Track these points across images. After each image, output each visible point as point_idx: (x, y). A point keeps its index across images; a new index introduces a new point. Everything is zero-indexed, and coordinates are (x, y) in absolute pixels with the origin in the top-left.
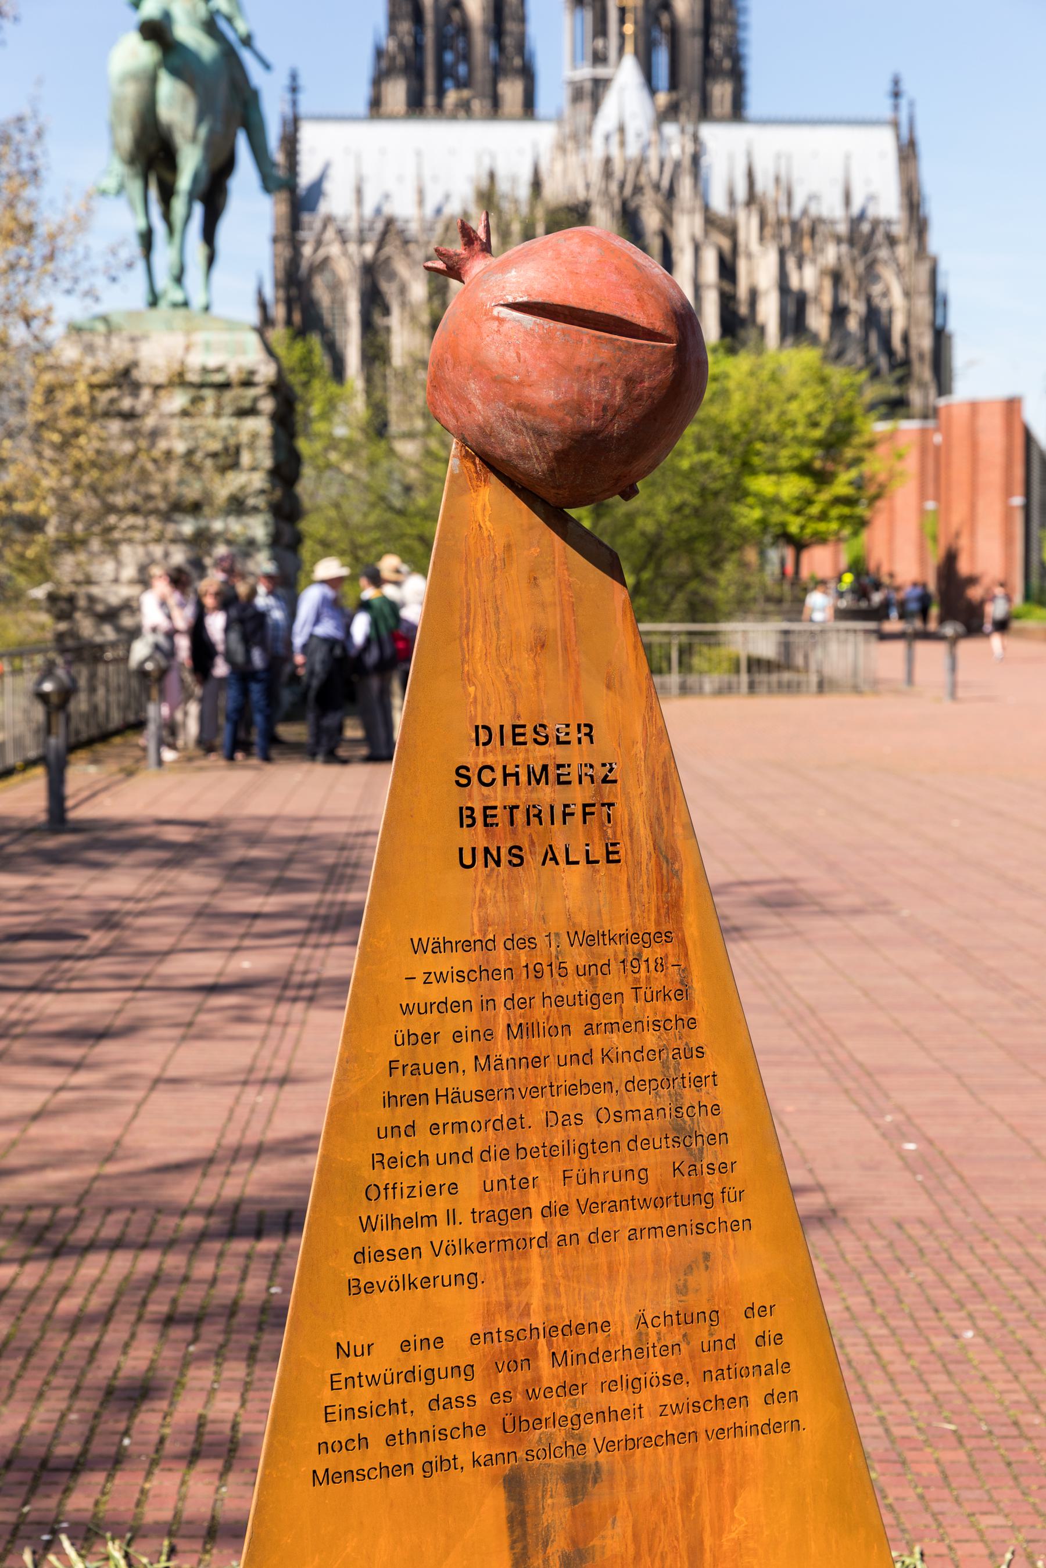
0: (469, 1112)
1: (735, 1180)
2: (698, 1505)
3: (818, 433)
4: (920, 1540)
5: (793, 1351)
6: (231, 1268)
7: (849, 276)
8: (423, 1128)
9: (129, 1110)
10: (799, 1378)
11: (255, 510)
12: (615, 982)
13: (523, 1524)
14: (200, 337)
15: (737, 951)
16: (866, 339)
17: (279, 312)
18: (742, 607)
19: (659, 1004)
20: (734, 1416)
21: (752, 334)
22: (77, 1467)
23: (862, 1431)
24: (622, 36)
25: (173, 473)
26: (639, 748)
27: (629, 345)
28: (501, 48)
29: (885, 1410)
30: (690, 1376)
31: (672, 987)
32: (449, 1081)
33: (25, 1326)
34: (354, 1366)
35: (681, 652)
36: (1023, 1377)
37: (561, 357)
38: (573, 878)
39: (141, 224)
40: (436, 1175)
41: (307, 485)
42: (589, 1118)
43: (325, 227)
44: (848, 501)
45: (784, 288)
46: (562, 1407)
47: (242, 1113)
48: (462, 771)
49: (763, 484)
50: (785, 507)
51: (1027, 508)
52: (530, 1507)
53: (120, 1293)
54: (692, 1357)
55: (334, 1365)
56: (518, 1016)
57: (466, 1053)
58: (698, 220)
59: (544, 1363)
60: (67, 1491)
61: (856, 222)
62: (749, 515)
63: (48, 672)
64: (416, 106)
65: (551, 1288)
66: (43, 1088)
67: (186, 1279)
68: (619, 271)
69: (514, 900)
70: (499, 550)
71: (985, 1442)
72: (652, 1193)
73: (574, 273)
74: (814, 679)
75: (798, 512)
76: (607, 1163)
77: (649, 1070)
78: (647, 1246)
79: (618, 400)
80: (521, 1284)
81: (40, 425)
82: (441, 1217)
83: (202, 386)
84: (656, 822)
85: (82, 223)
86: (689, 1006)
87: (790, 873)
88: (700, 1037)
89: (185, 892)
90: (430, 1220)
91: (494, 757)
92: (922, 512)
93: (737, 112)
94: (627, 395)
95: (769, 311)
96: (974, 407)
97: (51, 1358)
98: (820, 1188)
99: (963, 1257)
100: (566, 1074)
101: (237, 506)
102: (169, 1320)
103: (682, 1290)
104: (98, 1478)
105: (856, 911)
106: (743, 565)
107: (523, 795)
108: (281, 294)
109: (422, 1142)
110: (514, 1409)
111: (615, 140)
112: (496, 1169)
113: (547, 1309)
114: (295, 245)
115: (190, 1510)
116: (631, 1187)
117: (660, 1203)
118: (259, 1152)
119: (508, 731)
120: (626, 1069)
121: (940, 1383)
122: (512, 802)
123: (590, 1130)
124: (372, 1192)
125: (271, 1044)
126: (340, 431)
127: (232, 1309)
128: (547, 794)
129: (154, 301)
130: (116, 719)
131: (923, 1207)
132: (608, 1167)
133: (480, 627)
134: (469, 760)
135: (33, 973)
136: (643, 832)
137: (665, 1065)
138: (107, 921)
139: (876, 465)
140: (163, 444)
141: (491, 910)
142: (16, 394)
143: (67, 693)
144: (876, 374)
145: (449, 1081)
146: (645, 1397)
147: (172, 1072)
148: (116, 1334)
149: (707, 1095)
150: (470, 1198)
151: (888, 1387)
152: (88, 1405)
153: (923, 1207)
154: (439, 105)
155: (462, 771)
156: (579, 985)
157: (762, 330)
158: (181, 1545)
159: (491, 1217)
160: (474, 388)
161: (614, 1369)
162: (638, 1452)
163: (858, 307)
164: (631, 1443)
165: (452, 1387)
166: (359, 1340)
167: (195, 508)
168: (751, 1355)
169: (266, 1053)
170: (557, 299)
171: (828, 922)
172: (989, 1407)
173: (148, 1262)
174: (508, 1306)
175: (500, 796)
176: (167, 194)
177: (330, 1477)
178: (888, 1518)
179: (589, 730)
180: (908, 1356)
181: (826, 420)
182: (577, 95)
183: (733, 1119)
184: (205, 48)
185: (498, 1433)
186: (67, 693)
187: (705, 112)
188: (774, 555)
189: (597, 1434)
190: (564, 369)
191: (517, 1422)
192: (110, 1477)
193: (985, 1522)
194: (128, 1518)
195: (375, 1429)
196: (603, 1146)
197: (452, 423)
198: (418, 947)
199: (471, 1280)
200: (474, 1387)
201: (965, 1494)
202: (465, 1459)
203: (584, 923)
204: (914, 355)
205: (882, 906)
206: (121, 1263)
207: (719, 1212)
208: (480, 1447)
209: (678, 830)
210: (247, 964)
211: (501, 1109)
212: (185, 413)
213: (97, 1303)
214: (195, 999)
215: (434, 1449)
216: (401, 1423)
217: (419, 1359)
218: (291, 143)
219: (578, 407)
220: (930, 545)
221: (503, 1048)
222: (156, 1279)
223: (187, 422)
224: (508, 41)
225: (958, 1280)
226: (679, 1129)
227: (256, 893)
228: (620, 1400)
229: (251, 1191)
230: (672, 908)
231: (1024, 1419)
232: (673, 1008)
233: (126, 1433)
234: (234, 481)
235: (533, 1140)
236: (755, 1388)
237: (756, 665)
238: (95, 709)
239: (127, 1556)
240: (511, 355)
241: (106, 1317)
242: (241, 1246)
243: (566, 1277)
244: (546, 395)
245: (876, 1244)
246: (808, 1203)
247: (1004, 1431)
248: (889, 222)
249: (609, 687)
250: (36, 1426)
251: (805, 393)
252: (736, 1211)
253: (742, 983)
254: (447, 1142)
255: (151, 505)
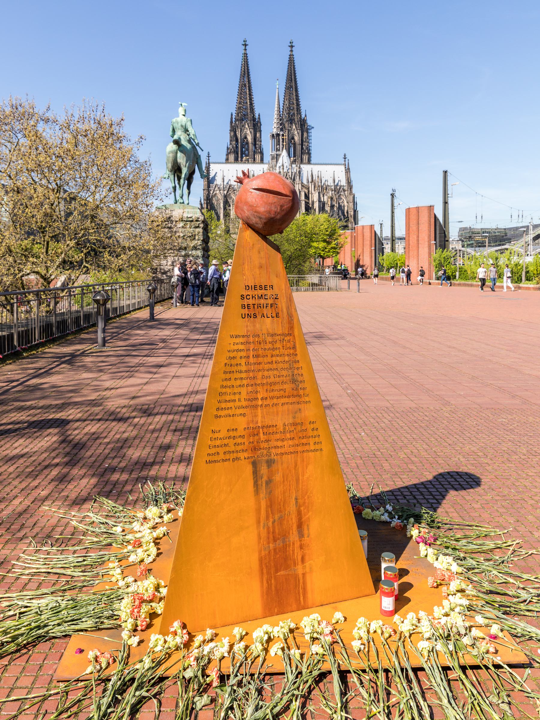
0: (244, 375)
1: (306, 392)
2: (298, 469)
3: (328, 233)
4: (352, 481)
5: (321, 432)
6: (190, 418)
7: (334, 198)
8: (233, 379)
9: (167, 383)
10: (322, 439)
11: (199, 249)
12: (278, 345)
13: (256, 473)
14: (186, 210)
15: (309, 347)
16: (339, 211)
17: (205, 206)
18: (310, 271)
19: (289, 350)
20: (306, 448)
21: (313, 211)
22: (153, 464)
23: (338, 456)
24: (283, 145)
25: (180, 240)
26: (284, 291)
27: (281, 198)
28: (255, 148)
29: (343, 451)
30: (296, 438)
31: (291, 347)
32: (239, 368)
33: (141, 432)
34: (216, 435)
35: (296, 282)
36: (376, 444)
37: (265, 200)
38: (268, 321)
39: (173, 185)
40: (236, 390)
41: (210, 244)
42: (272, 377)
43: (216, 187)
44: (335, 248)
45: (320, 201)
46: (266, 445)
47: (193, 384)
48: (242, 296)
49: (315, 244)
50: (320, 249)
51: (375, 250)
52: (258, 469)
53: (164, 425)
54: (296, 433)
55: (211, 435)
56: (255, 353)
57: (243, 361)
58: (300, 186)
59: (261, 435)
60: (150, 470)
61: (336, 186)
62: (312, 251)
63: (150, 285)
64: (236, 160)
65: (263, 417)
66: (147, 378)
67: (179, 421)
68: (279, 181)
69: (254, 326)
70: (251, 245)
71: (367, 458)
72: (287, 394)
73: (268, 182)
74: (327, 288)
75: (323, 251)
76: (277, 387)
77: (286, 366)
78: (286, 407)
79: (279, 211)
80: (256, 416)
81: (150, 229)
82: (237, 400)
83: (187, 221)
84: (288, 308)
85: (159, 184)
86: (296, 351)
87: (322, 330)
88: (298, 358)
89: (181, 334)
90: (235, 401)
91: (250, 292)
92: (352, 251)
93: (309, 162)
94: (281, 209)
95: (316, 206)
96: (363, 226)
97: (147, 439)
98: (328, 400)
99: (362, 416)
100: (267, 367)
101: (195, 248)
102: (175, 431)
103: (294, 417)
104: (157, 467)
105: (336, 339)
106: (310, 262)
107: (257, 302)
108: (205, 202)
109: (233, 382)
110: (254, 446)
111: (281, 168)
112: (250, 389)
113: (262, 422)
114: (209, 191)
115: (179, 474)
116: (282, 393)
117: (289, 397)
118: (197, 392)
119: (253, 287)
120: (281, 365)
121: (356, 445)
122: (254, 303)
123: (272, 380)
124: (221, 394)
125: (201, 368)
126: (219, 232)
127: (190, 428)
128: (262, 301)
129: (176, 203)
130: (166, 297)
131: (352, 405)
132: (277, 388)
133: (247, 263)
134: (244, 293)
135: (146, 352)
136: (285, 310)
137: (290, 364)
138: (164, 341)
139: (341, 240)
140: (178, 234)
141: (249, 328)
142: (144, 222)
143: (155, 289)
144: (341, 220)
145: (239, 368)
146: (285, 443)
147: (177, 375)
148: (162, 434)
149: (300, 372)
150: (244, 395)
151: (344, 446)
152: (155, 450)
153: (352, 405)
154: (242, 160)
155: (242, 296)
156: (270, 346)
157: (315, 210)
158: (176, 483)
159: (249, 400)
160: (245, 208)
161: (278, 436)
162: (284, 456)
163: (337, 205)
164: (282, 454)
165: (239, 440)
166: (217, 429)
167: (185, 249)
168: (311, 433)
169: (199, 370)
170: (264, 188)
171: (330, 341)
172: (368, 450)
173: (171, 417)
174: (253, 421)
175: (251, 302)
176: (179, 179)
177: (210, 462)
178: (344, 476)
179: (271, 286)
180: (349, 439)
181: (329, 230)
182: (273, 158)
183: (306, 377)
184: (189, 146)
185: (250, 452)
186: (155, 289)
187: (302, 162)
188: (318, 260)
189: (274, 452)
190: (266, 203)
191: (255, 449)
192: (160, 467)
193: (367, 477)
194: (164, 476)
195: (221, 450)
196: (275, 384)
197: (240, 216)
198: (232, 337)
199: (244, 415)
200: (245, 440)
201: (362, 471)
202: (242, 458)
203: (271, 331)
204: (349, 216)
205: (343, 338)
206: (164, 417)
207: (303, 399)
208: (246, 455)
209: (293, 310)
210: (195, 351)
211: (251, 375)
212: (183, 227)
213: (158, 427)
214: (183, 358)
215: (235, 455)
216: (227, 449)
217: (232, 434)
218: (208, 168)
219: (269, 212)
220: (353, 258)
221: (252, 360)
222: (172, 421)
223: (183, 230)
224: (257, 146)
225: (360, 421)
226: (293, 380)
227: (198, 335)
228: (279, 444)
229: (195, 401)
230: (291, 328)
231: (376, 453)
232: (292, 351)
233: (164, 457)
234: (194, 243)
235: (259, 382)
236: (312, 441)
237: (313, 285)
238: (161, 293)
239: (163, 485)
240: (254, 200)
241: (160, 430)
242: (193, 413)
243: (267, 414)
244: (262, 209)
245: (341, 413)
246: (325, 404)
247: (371, 456)
248: (344, 186)
249: (277, 277)
250: (143, 455)
251: (324, 223)
252: (307, 399)
253: (310, 355)
254: (238, 382)
255: (175, 248)
